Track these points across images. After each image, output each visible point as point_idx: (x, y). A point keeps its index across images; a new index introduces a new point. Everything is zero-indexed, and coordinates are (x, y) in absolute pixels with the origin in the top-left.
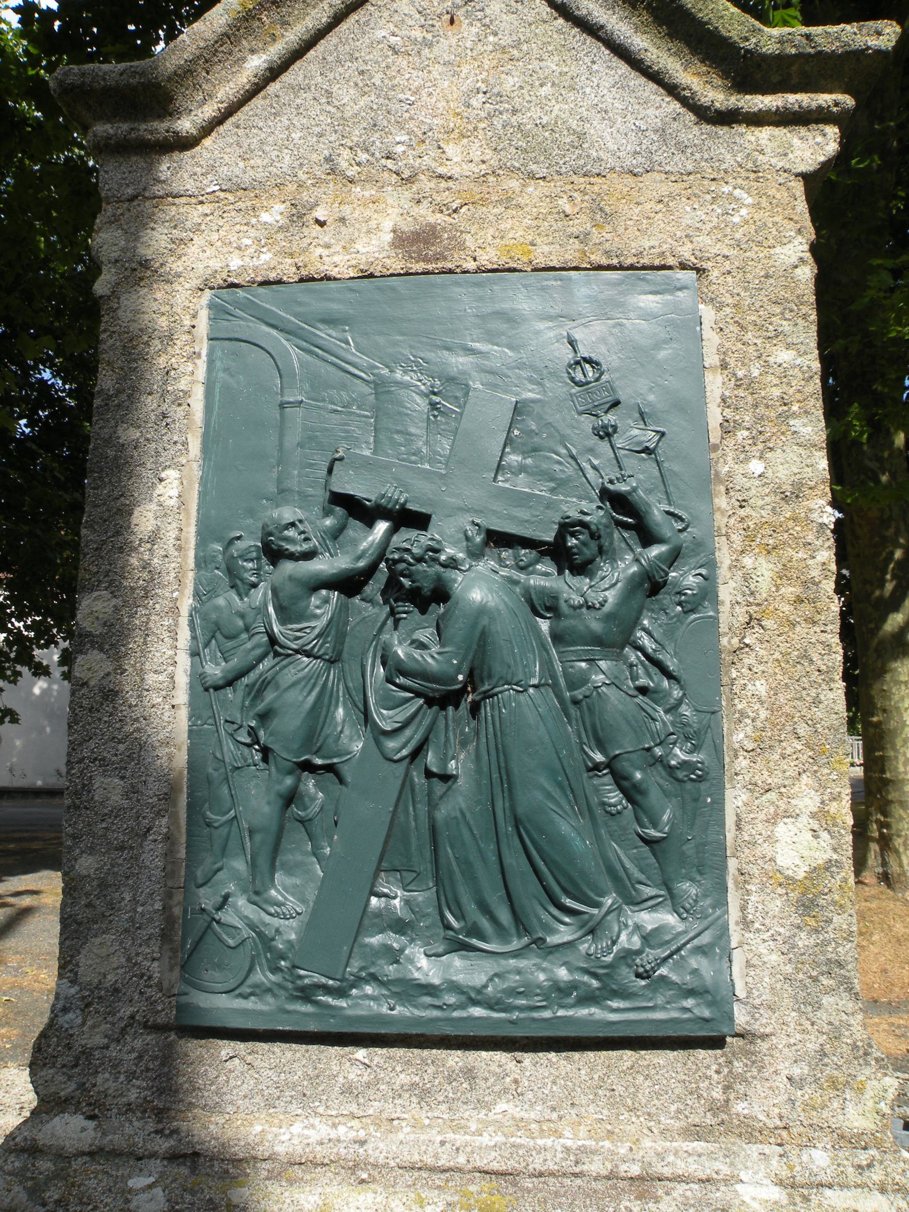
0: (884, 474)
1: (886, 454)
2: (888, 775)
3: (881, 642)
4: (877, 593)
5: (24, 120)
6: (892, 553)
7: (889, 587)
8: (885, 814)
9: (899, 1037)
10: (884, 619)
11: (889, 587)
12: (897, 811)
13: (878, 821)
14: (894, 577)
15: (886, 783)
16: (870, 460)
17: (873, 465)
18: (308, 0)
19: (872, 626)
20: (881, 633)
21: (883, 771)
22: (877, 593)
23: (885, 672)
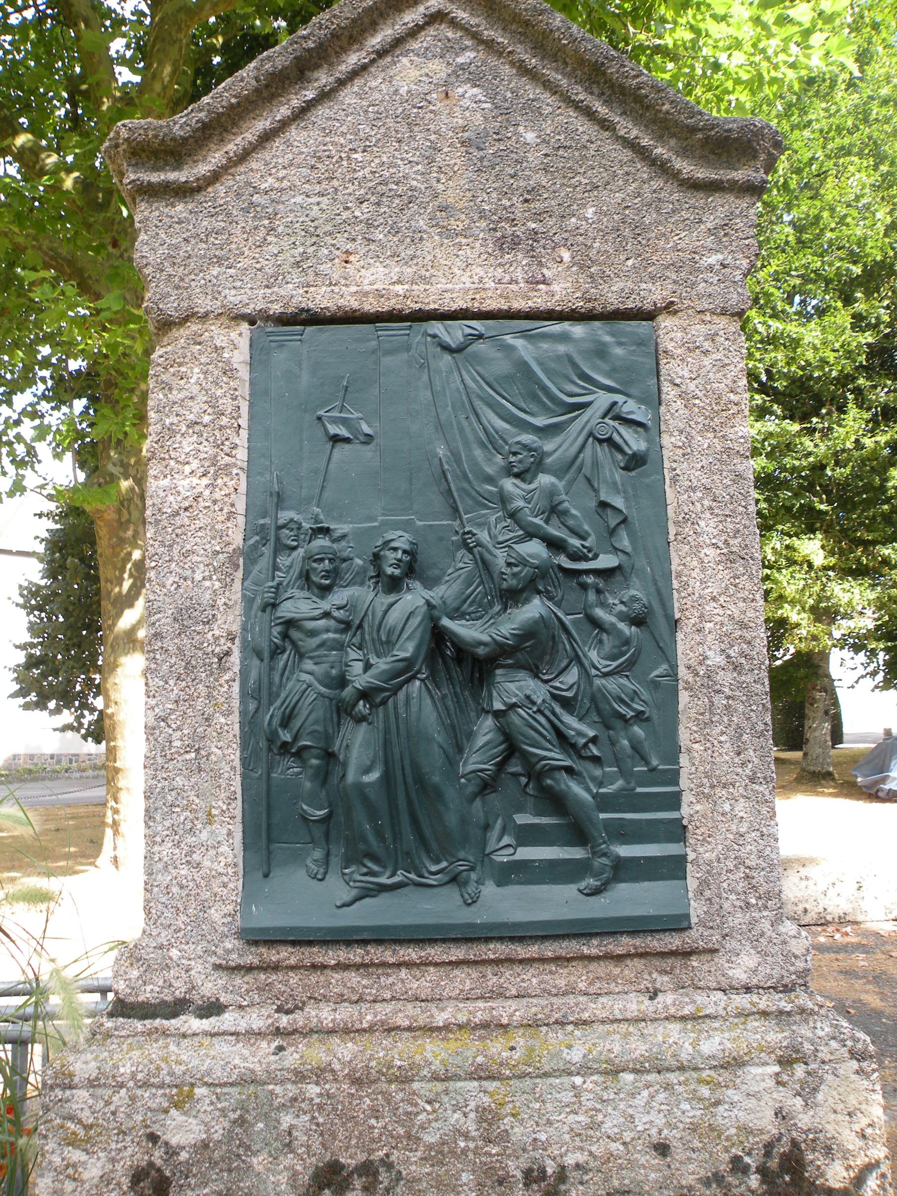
0: (126, 479)
1: (132, 461)
2: (118, 764)
3: (116, 638)
4: (117, 590)
5: (121, 212)
6: (130, 554)
7: (127, 584)
8: (116, 801)
9: (356, 1002)
10: (119, 615)
11: (127, 584)
12: (122, 796)
13: (112, 808)
14: (131, 576)
15: (117, 771)
16: (115, 465)
17: (116, 470)
18: (896, 236)
19: (110, 622)
20: (116, 629)
21: (115, 761)
22: (117, 590)
23: (117, 666)
